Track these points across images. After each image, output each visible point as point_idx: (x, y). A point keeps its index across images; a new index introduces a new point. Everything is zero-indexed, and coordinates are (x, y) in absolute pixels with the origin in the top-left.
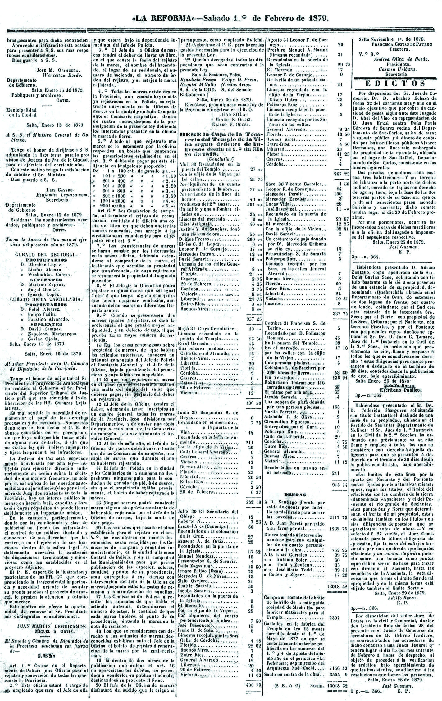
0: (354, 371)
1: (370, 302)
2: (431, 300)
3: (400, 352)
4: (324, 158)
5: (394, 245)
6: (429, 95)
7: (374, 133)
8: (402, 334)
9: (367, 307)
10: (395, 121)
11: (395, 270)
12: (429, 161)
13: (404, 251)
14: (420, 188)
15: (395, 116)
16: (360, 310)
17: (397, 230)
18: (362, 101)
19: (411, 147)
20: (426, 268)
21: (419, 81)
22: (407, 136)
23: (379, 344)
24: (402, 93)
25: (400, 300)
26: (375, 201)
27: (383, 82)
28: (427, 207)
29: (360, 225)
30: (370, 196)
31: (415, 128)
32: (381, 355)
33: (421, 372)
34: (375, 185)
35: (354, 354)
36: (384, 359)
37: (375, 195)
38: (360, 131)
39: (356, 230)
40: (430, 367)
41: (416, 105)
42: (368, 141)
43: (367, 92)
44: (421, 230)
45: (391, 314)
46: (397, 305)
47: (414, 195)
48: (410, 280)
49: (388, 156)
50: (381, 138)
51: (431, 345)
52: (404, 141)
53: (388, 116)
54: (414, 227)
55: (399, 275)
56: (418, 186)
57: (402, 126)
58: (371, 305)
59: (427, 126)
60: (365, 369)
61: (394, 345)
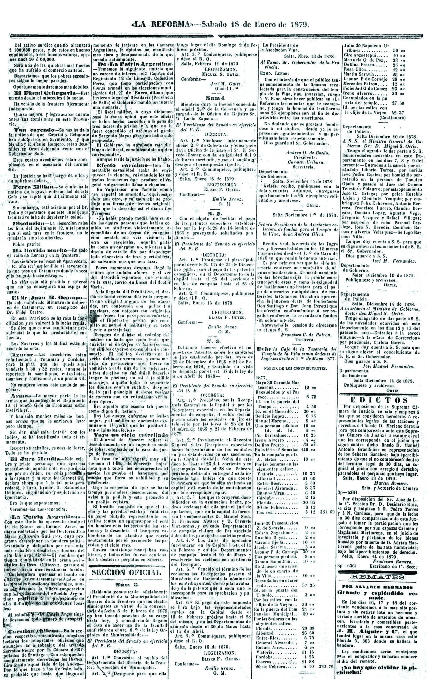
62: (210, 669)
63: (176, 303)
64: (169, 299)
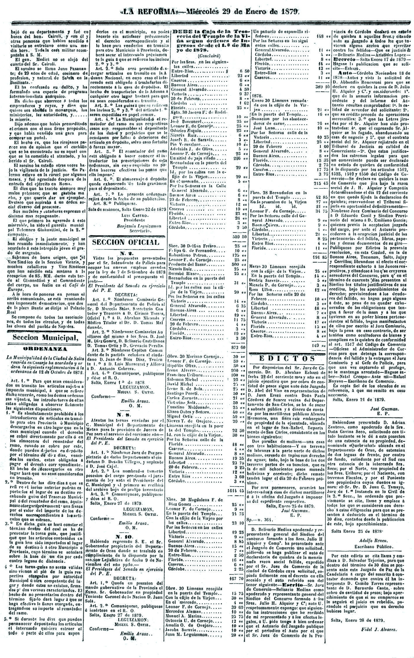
0: (330, 519)
1: (345, 455)
2: (402, 453)
3: (373, 501)
4: (303, 317)
5: (285, 509)
6: (318, 370)
7: (267, 405)
8: (375, 484)
9: (342, 459)
10: (287, 393)
11: (368, 425)
12: (318, 431)
13: (295, 514)
14: (310, 456)
15: (287, 389)
16: (336, 462)
17: (288, 495)
18: (256, 375)
19: (301, 417)
20: (396, 423)
21: (309, 357)
22: (298, 407)
23: (353, 494)
24: (293, 367)
25: (373, 453)
26: (268, 468)
27: (275, 357)
28: (317, 474)
29: (254, 490)
30: (264, 463)
31: (305, 400)
32: (356, 504)
33: (392, 520)
34: (269, 453)
35: (330, 503)
36: (358, 508)
37: (268, 462)
38: (254, 402)
39: (250, 495)
40: (401, 515)
41: (306, 379)
42: (261, 412)
43: (261, 366)
44: (310, 495)
45: (365, 466)
46: (370, 457)
47: (305, 463)
48: (382, 434)
49: (280, 426)
50: (273, 409)
51: (402, 494)
52: (295, 412)
53: (281, 389)
54: (305, 493)
55: (371, 430)
56: (308, 454)
57: (293, 398)
58: (346, 457)
59: (317, 398)
60: (341, 517)
61: (367, 494)
62: (124, 523)
63: (88, 503)
64: (82, 500)
